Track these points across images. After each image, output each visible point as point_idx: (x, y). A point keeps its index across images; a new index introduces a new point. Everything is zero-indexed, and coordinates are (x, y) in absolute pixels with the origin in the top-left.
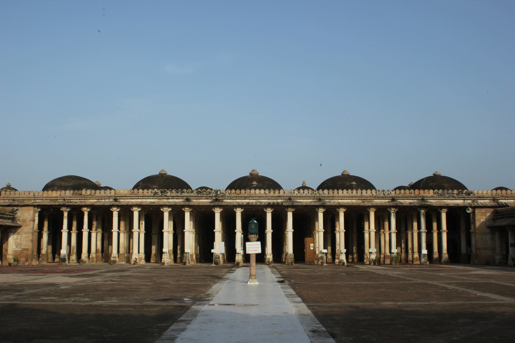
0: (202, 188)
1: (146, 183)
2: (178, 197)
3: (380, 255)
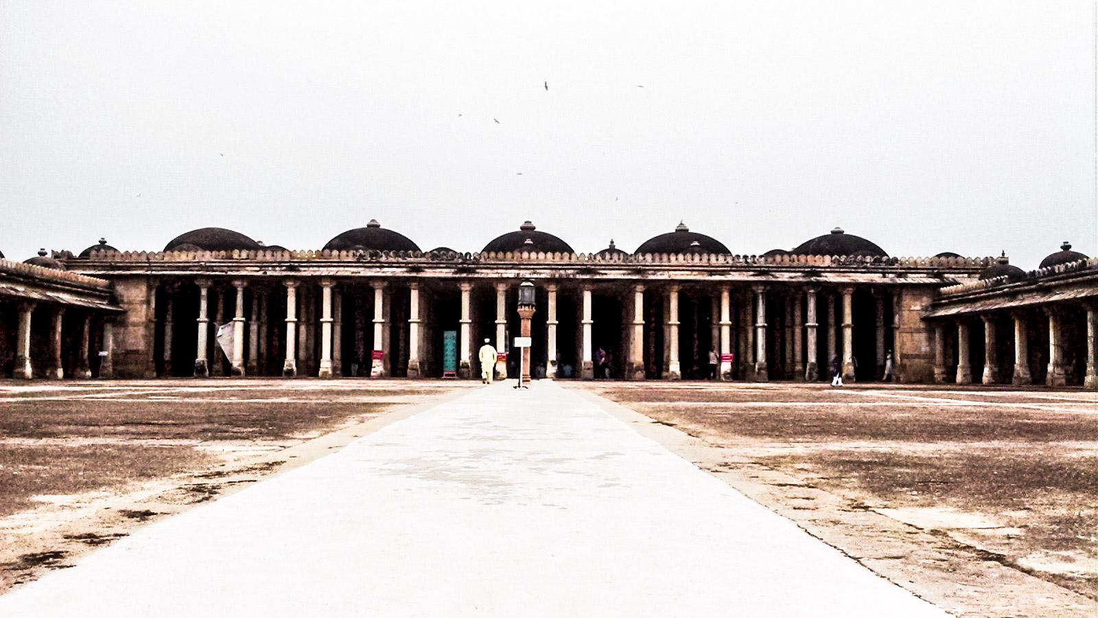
0: (439, 250)
1: (345, 241)
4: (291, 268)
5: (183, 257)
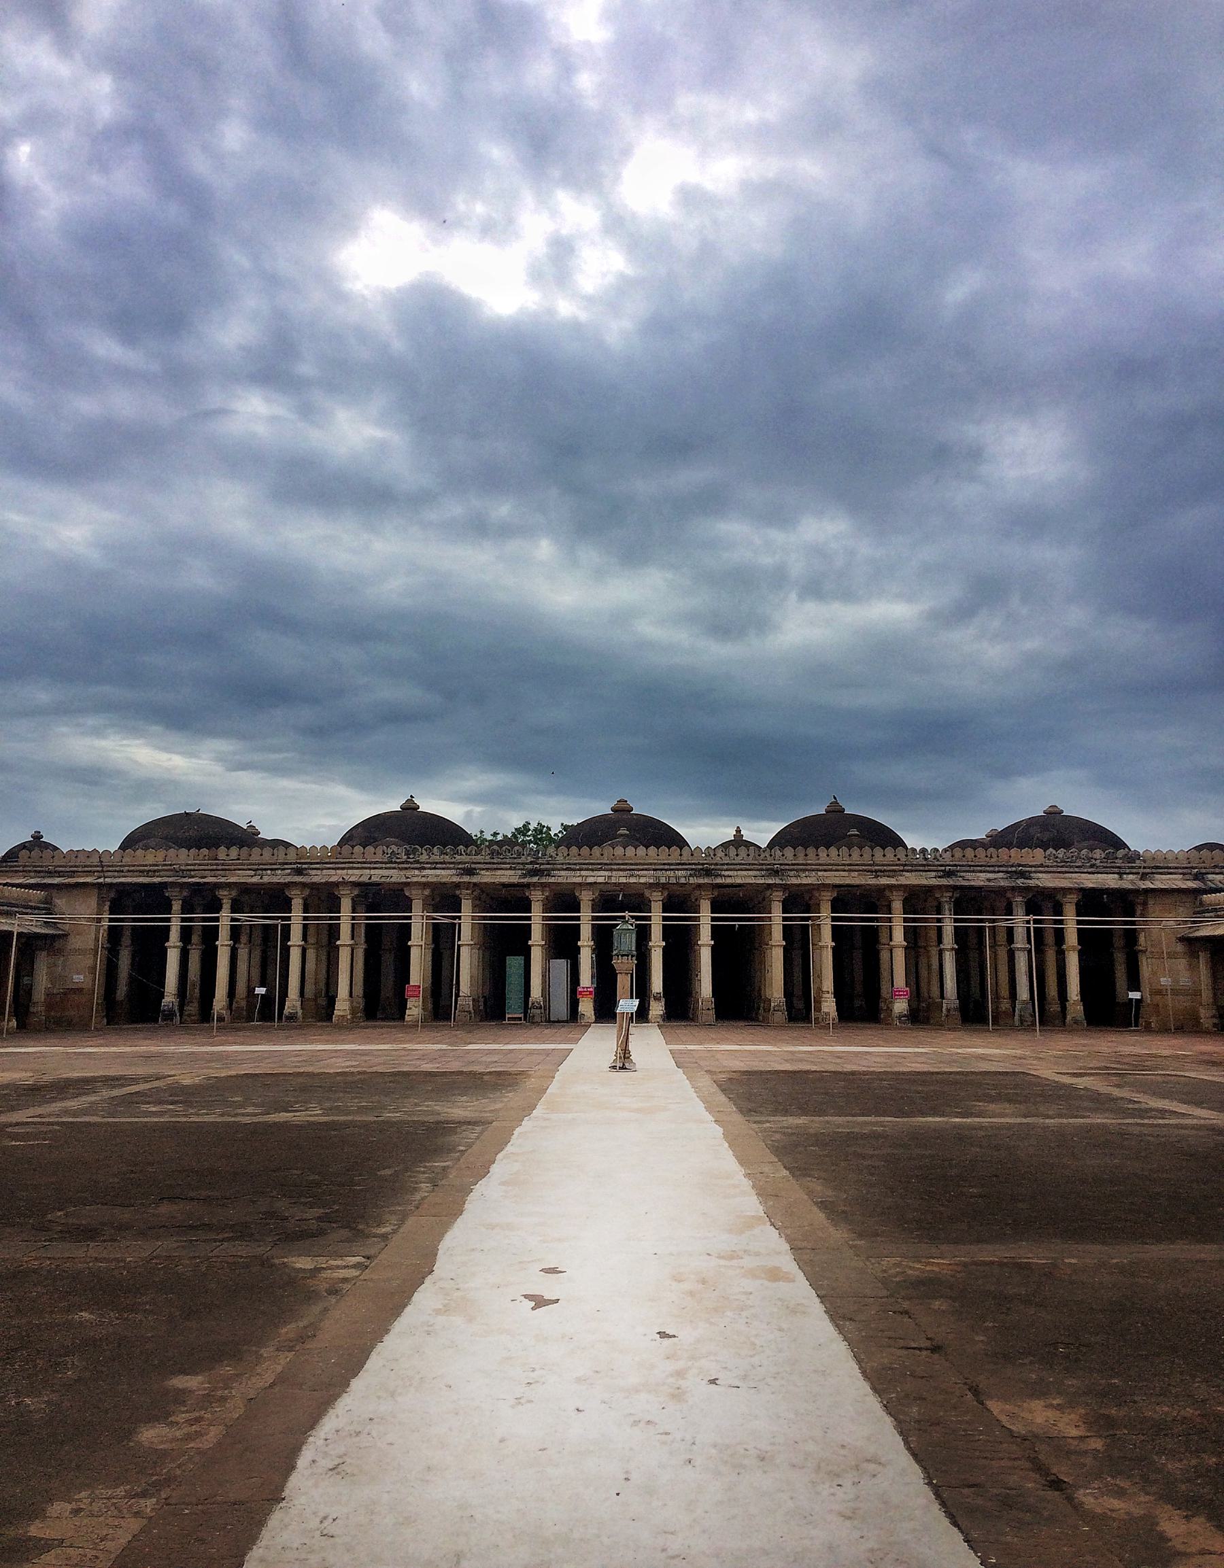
2: (444, 865)
3: (919, 1001)
4: (299, 872)
5: (151, 857)
